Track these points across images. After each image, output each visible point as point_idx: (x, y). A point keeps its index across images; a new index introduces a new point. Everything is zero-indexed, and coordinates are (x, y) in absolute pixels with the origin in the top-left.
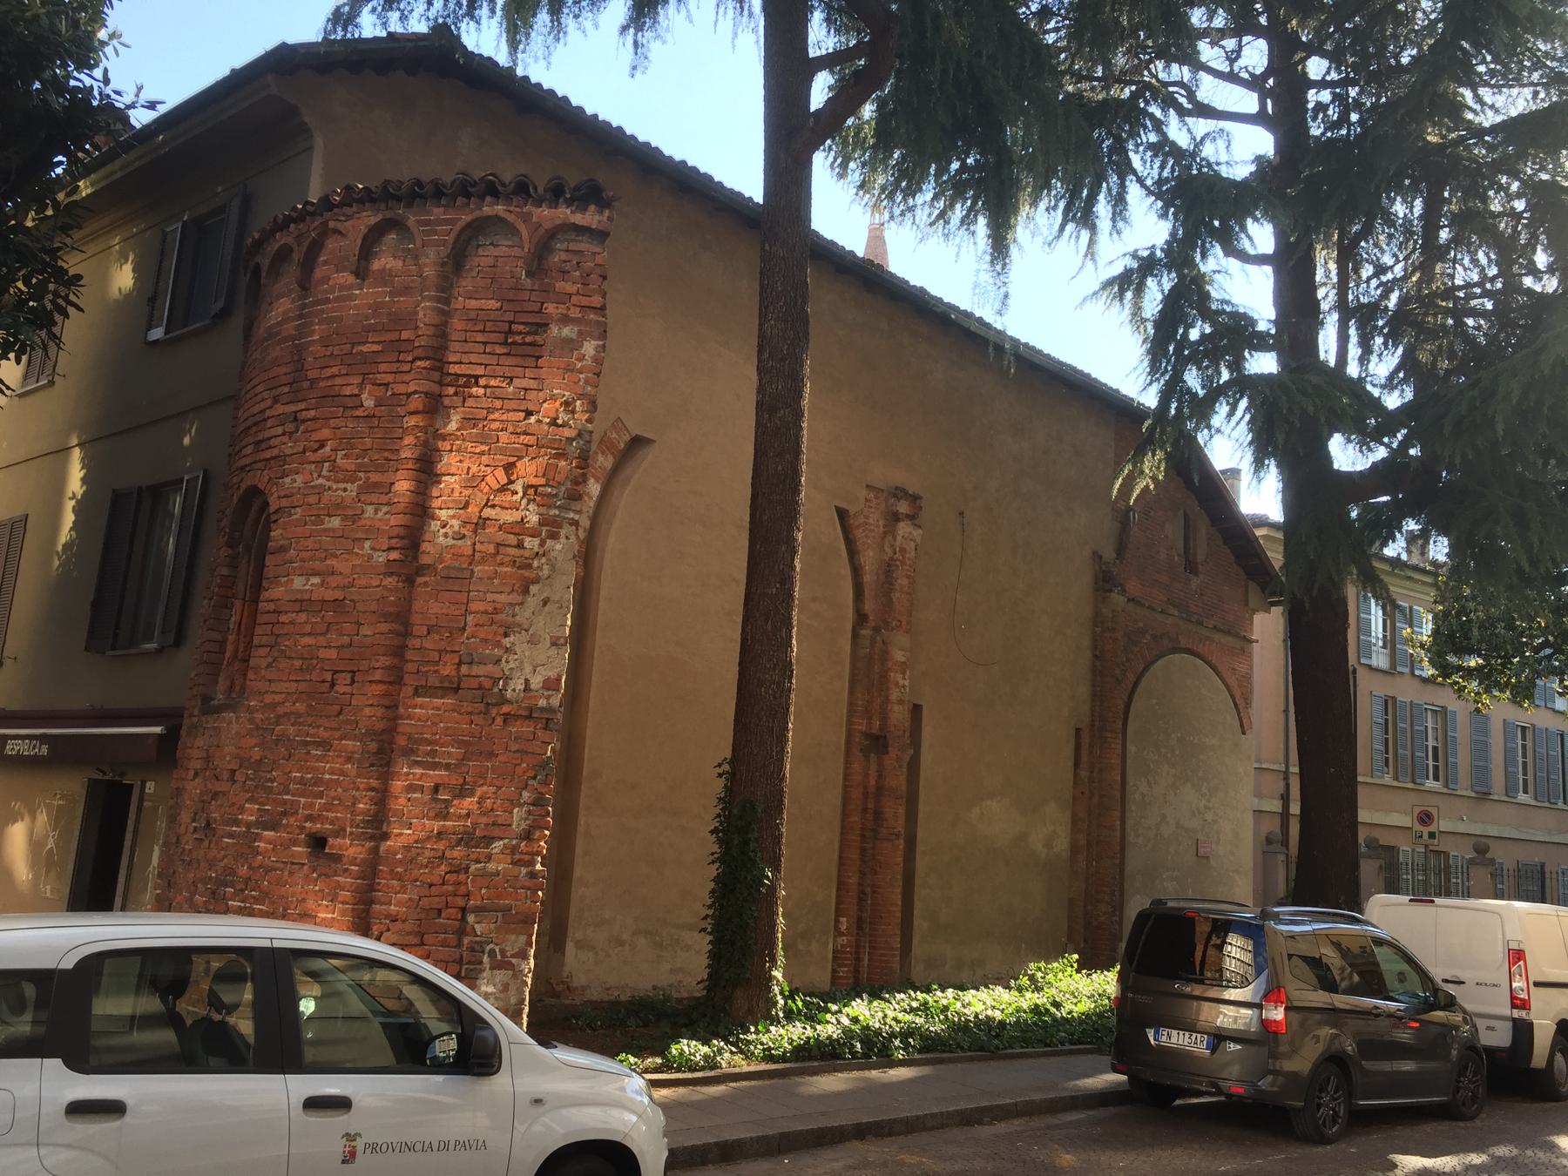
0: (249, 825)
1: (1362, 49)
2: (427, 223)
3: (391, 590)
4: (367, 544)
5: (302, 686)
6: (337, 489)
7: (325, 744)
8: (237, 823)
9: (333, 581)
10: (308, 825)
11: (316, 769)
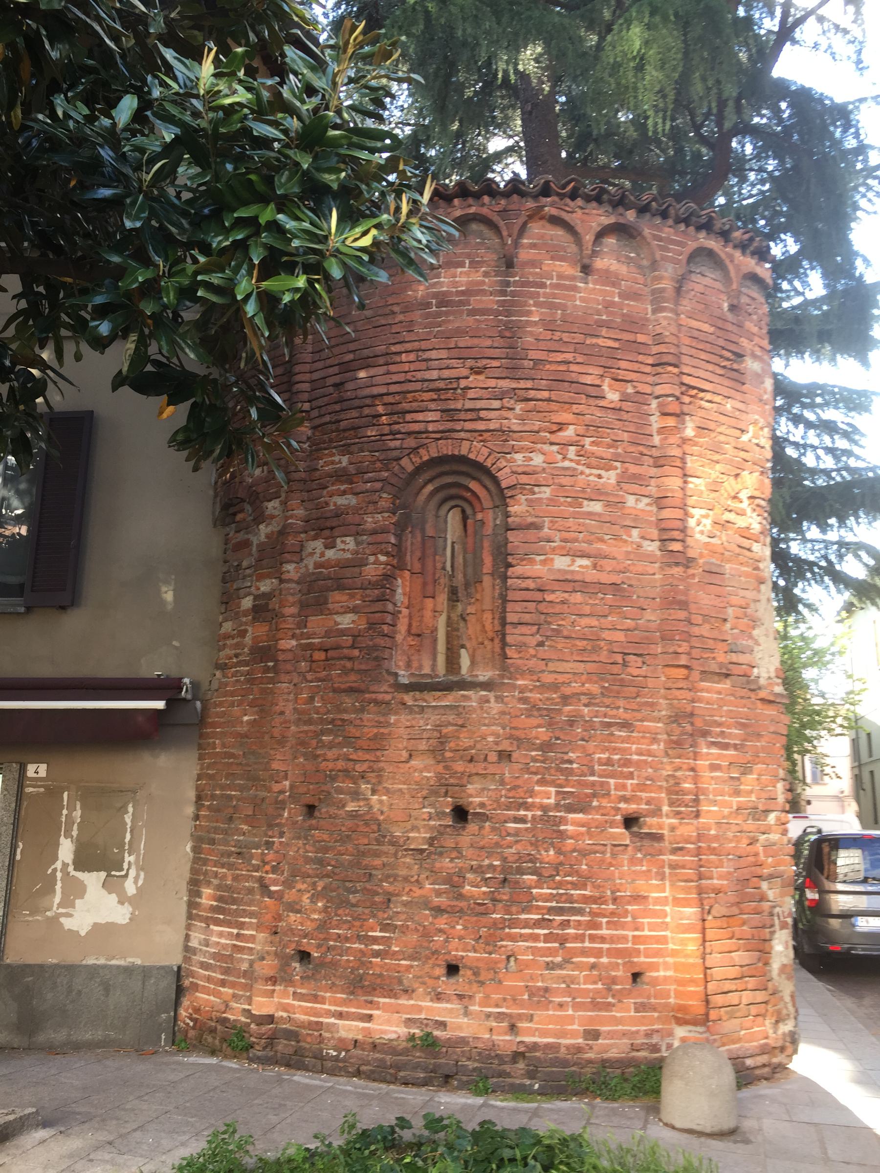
0: (545, 808)
1: (154, 186)
2: (660, 239)
3: (680, 580)
4: (635, 533)
5: (590, 667)
6: (590, 475)
7: (626, 725)
8: (527, 807)
9: (608, 565)
10: (622, 805)
11: (623, 751)
